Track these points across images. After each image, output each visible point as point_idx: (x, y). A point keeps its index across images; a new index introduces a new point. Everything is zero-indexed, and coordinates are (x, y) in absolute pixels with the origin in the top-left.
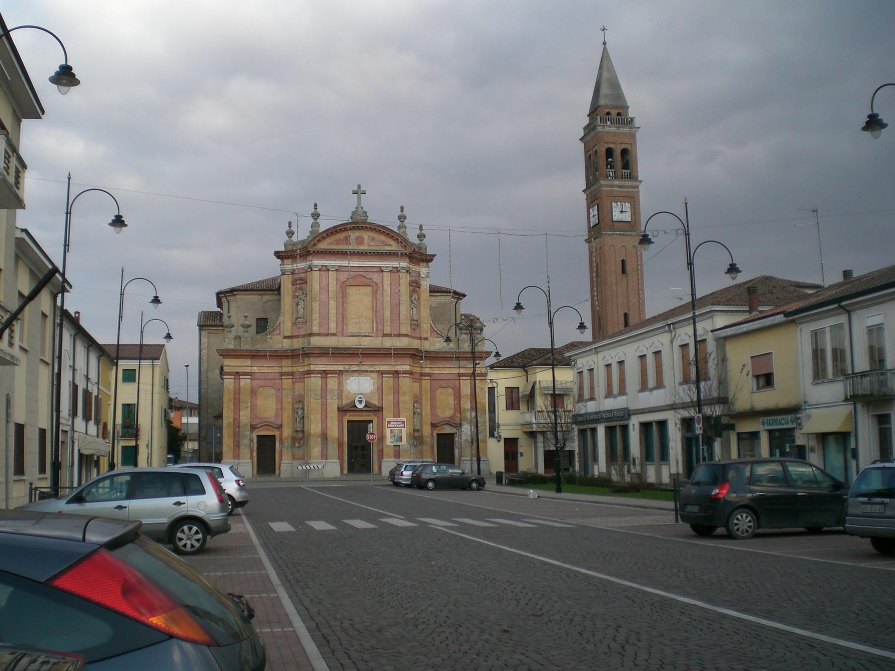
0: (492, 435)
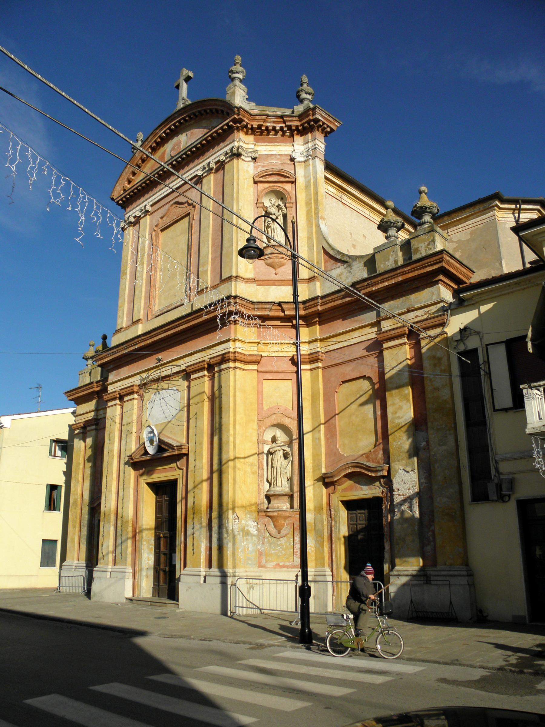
0: (480, 496)
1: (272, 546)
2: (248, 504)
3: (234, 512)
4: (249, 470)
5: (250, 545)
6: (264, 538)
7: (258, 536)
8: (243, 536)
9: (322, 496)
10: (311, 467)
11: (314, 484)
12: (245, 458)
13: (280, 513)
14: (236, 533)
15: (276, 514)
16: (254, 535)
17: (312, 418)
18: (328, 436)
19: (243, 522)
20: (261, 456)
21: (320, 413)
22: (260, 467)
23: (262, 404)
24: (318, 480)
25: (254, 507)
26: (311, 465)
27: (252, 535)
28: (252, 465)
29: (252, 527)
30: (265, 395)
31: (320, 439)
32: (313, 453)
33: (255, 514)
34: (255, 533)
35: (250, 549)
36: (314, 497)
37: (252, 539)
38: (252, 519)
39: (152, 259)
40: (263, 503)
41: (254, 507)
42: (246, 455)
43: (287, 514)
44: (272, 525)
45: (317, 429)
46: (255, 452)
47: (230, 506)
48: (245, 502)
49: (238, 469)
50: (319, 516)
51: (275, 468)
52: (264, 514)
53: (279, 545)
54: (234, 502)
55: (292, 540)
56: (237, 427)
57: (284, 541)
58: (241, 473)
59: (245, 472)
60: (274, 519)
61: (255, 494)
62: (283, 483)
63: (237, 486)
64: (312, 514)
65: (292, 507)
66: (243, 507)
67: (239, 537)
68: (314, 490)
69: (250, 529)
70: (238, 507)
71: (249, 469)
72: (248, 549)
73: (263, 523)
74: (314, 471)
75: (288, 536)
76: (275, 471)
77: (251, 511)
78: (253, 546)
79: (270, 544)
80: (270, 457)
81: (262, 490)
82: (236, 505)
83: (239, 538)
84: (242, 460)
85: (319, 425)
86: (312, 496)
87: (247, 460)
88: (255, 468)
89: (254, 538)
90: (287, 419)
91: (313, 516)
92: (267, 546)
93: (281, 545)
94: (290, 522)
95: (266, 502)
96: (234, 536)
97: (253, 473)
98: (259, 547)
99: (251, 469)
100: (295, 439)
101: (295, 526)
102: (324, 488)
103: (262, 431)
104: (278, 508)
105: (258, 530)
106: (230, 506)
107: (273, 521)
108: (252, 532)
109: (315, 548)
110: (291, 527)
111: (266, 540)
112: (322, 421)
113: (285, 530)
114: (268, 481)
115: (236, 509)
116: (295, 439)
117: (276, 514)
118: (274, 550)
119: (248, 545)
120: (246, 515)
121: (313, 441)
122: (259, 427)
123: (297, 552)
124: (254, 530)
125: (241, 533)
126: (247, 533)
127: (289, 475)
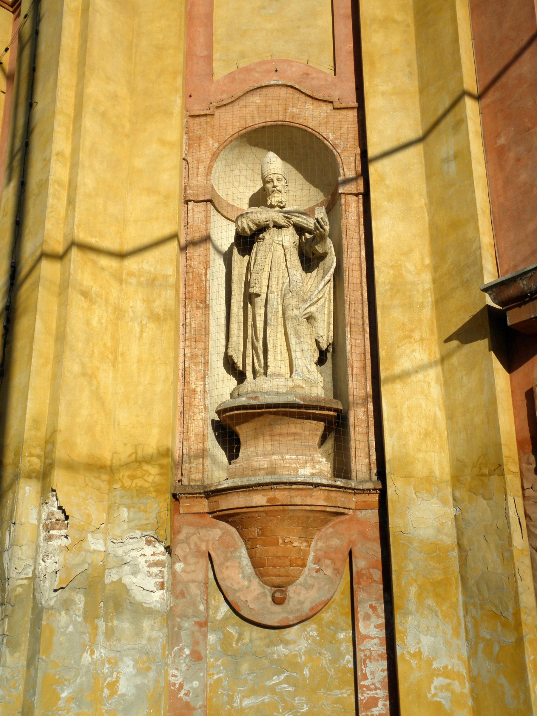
1: (245, 667)
2: (125, 453)
3: (47, 490)
4: (140, 306)
5: (128, 667)
6: (202, 624)
7: (170, 617)
8: (90, 615)
9: (493, 402)
10: (428, 285)
11: (443, 360)
12: (122, 256)
13: (281, 496)
14: (48, 598)
15: (259, 499)
16: (150, 612)
17: (422, 91)
18: (502, 141)
19: (96, 543)
20: (196, 253)
21: (457, 51)
22: (195, 295)
23: (209, 59)
24: (465, 335)
25: (153, 470)
26: (427, 277)
27: (140, 611)
28: (152, 282)
29: (142, 571)
30: (220, 30)
31: (463, 156)
32: (433, 227)
33: (158, 506)
34: (157, 598)
35: (123, 687)
36: (450, 417)
37: (139, 633)
38: (141, 528)
39: (196, 493)
40: (203, 454)
41: (153, 470)
42: (128, 247)
43: (318, 499)
44: (246, 561)
45: (450, 119)
46: (168, 230)
47: (31, 461)
48: (113, 447)
49: (85, 294)
50: (480, 509)
51: (260, 301)
52: (204, 506)
53: (279, 666)
54: (50, 441)
55: (345, 635)
56: (89, 122)
57: (303, 645)
58: (99, 316)
59: (119, 313)
60: (254, 531)
61: (162, 411)
62: (298, 363)
63: (72, 366)
64: (444, 502)
65: (342, 468)
66: (96, 467)
67: (63, 618)
68: (447, 383)
69: (127, 580)
70: (71, 466)
71: (136, 303)
72: (113, 686)
73: (198, 553)
74: (440, 301)
75: (327, 616)
76: (260, 311)
77: (141, 492)
78: (141, 672)
79: (233, 656)
80: (239, 262)
81: (199, 396)
82: (60, 453)
83: (65, 624)
84: (105, 261)
85: (457, 101)
86: (440, 415)
87: (131, 264)
88: (167, 298)
89: (146, 624)
90: (310, 105)
91: (451, 511)
92: (217, 670)
93: (293, 665)
94: (335, 542)
95: (221, 455)
96: (38, 612)
97: (155, 318)
98: (176, 676)
99: (148, 301)
100: (347, 181)
101: (360, 564)
102: (497, 364)
103: (205, 155)
104: (272, 471)
105: (175, 587)
106: (31, 461)
107: (246, 539)
108: (139, 596)
109: (473, 679)
110: (337, 571)
111: (212, 638)
112: (470, 83)
113: (308, 587)
114: (230, 365)
115: (59, 478)
116: (347, 181)
117: (259, 499)
118: (253, 692)
119: (114, 664)
120: (110, 509)
121: (429, 177)
122: (192, 140)
123: (373, 702)
124: (151, 583)
125: (80, 600)
126: (104, 598)
127: (324, 331)
